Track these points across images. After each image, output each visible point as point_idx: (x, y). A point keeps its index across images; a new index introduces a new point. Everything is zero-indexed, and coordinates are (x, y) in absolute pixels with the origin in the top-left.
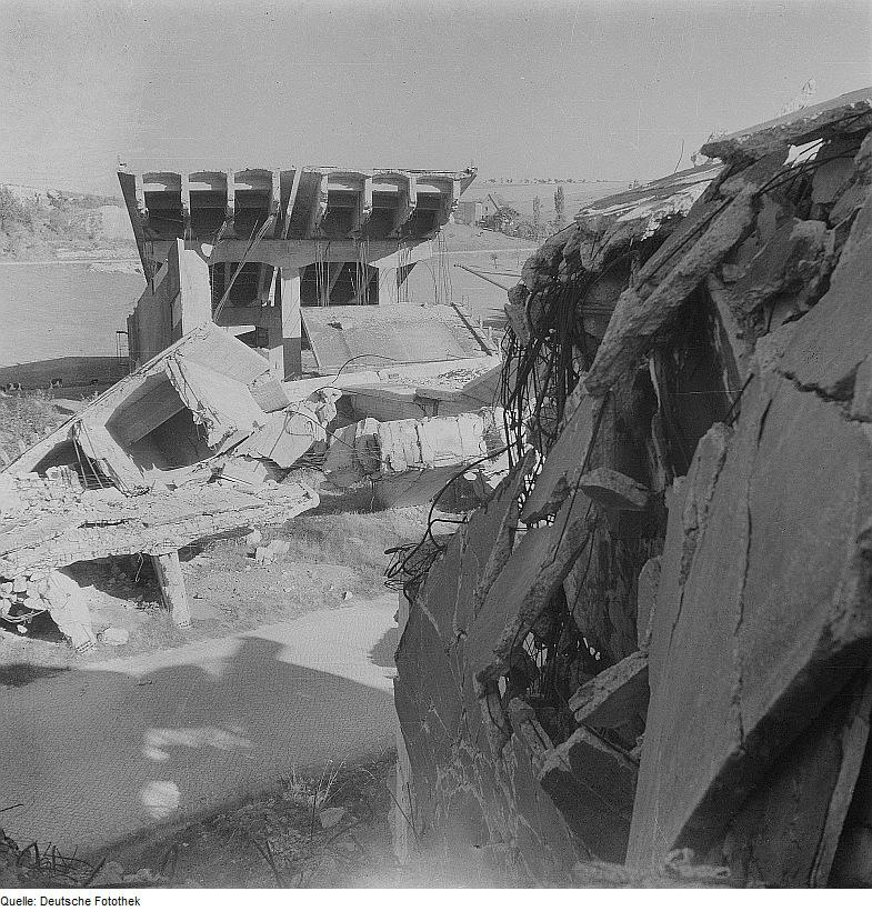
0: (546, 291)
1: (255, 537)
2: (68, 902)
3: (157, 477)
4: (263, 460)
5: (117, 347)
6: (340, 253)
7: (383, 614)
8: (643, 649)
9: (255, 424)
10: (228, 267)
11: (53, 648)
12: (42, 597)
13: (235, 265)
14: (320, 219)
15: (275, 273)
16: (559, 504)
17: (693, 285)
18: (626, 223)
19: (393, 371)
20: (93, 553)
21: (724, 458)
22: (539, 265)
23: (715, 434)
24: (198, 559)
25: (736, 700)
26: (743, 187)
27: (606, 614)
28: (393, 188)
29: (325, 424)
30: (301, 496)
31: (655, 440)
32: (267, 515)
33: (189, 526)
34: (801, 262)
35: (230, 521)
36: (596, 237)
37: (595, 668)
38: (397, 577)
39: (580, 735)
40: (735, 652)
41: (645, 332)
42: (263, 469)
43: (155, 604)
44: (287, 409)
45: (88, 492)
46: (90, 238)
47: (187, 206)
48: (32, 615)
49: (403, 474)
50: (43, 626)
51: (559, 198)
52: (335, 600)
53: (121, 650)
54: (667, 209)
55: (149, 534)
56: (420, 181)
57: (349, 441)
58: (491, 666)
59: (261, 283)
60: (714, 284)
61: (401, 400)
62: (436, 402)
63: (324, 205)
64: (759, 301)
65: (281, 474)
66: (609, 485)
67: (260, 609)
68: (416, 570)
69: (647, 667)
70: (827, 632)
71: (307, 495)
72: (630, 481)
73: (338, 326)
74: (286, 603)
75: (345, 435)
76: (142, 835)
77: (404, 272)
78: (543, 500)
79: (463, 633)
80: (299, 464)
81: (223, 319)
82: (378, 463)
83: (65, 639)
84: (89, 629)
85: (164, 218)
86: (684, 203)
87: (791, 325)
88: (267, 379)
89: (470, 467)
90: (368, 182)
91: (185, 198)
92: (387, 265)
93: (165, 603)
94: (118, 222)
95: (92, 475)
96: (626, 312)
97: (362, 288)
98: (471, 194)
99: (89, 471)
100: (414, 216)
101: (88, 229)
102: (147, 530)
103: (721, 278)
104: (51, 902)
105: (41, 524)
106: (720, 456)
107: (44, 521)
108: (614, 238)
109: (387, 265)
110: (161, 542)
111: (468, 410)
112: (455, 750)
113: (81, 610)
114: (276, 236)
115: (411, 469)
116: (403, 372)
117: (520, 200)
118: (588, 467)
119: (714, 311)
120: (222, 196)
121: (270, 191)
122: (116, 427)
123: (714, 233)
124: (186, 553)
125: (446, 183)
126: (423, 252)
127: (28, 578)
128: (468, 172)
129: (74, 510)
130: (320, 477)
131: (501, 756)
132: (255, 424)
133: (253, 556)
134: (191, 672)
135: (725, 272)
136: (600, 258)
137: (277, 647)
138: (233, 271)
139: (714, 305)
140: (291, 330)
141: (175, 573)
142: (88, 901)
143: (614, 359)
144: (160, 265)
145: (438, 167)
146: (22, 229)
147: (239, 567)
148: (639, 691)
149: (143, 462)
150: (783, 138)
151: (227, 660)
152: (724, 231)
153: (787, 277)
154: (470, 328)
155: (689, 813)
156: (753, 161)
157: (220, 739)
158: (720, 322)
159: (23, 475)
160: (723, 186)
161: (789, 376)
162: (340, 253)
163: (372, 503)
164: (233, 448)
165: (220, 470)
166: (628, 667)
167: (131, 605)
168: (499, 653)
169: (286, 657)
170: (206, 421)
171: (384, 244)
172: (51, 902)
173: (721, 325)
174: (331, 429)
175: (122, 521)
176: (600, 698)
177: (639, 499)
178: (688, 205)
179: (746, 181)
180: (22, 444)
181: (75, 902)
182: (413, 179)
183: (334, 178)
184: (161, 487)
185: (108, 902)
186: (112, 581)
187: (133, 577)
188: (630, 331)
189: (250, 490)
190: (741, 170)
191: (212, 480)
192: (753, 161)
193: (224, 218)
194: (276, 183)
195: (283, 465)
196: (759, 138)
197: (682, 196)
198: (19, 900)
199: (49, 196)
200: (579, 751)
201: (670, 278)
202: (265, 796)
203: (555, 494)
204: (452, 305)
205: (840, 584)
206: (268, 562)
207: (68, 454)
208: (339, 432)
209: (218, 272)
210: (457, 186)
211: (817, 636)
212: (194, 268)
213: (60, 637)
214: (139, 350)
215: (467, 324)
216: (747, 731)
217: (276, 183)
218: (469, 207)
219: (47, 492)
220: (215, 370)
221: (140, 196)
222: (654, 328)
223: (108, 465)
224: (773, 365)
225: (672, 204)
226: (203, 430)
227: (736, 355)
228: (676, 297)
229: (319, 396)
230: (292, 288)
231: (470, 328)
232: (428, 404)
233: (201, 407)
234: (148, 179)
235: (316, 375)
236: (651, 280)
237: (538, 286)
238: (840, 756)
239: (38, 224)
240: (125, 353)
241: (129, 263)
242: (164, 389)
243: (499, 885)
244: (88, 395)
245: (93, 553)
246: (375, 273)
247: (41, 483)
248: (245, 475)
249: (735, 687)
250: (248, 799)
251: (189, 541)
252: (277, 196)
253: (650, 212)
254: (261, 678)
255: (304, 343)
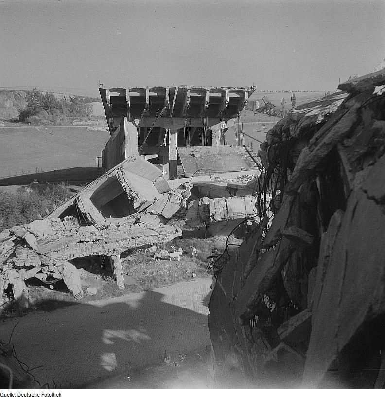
0: (276, 145)
1: (154, 248)
2: (30, 395)
3: (112, 221)
4: (158, 214)
6: (195, 123)
7: (205, 285)
9: (155, 199)
10: (146, 129)
11: (64, 295)
12: (60, 273)
13: (149, 129)
14: (186, 108)
15: (167, 132)
16: (277, 241)
18: (309, 117)
19: (217, 175)
20: (83, 254)
21: (340, 226)
22: (274, 134)
24: (129, 258)
26: (355, 104)
28: (219, 95)
29: (186, 199)
30: (173, 231)
34: (376, 139)
35: (142, 241)
36: (296, 122)
37: (294, 313)
39: (281, 345)
42: (158, 219)
44: (169, 192)
45: (82, 227)
46: (87, 116)
47: (129, 102)
48: (56, 281)
49: (219, 222)
50: (61, 286)
51: (293, 99)
52: (188, 277)
53: (93, 297)
54: (327, 111)
55: (107, 247)
56: (230, 92)
58: (246, 312)
59: (160, 137)
60: (340, 147)
63: (188, 102)
64: (358, 156)
65: (165, 221)
67: (155, 280)
68: (220, 265)
69: (310, 318)
70: (371, 308)
71: (177, 231)
72: (305, 233)
73: (194, 156)
74: (167, 278)
75: (194, 204)
77: (223, 132)
80: (174, 216)
81: (143, 152)
82: (209, 217)
83: (70, 292)
84: (80, 288)
85: (118, 108)
86: (333, 108)
87: (371, 167)
88: (161, 179)
90: (208, 92)
91: (128, 99)
92: (216, 128)
93: (114, 277)
94: (99, 109)
95: (84, 220)
96: (305, 156)
97: (205, 139)
98: (253, 97)
99: (82, 219)
101: (86, 112)
102: (107, 245)
103: (343, 144)
104: (22, 395)
106: (338, 224)
107: (62, 240)
108: (304, 123)
109: (216, 128)
110: (113, 250)
111: (248, 194)
113: (77, 280)
114: (167, 116)
115: (223, 220)
117: (276, 100)
118: (287, 225)
119: (339, 159)
120: (144, 98)
121: (165, 97)
123: (339, 125)
124: (123, 255)
125: (242, 93)
126: (231, 123)
127: (55, 265)
130: (183, 222)
134: (124, 306)
135: (345, 142)
136: (298, 131)
137: (161, 295)
139: (340, 156)
140: (173, 157)
141: (119, 264)
142: (39, 394)
143: (296, 179)
144: (116, 128)
145: (238, 86)
146: (59, 112)
147: (147, 262)
148: (307, 327)
149: (106, 214)
150: (373, 83)
151: (139, 301)
152: (343, 126)
154: (252, 157)
156: (360, 92)
158: (343, 164)
159: (54, 220)
161: (366, 192)
162: (195, 123)
163: (206, 234)
164: (145, 209)
166: (304, 315)
167: (99, 277)
169: (166, 300)
170: (133, 197)
171: (213, 120)
172: (22, 395)
174: (188, 202)
175: (96, 241)
176: (290, 329)
178: (336, 109)
180: (55, 206)
181: (33, 395)
182: (227, 91)
183: (193, 91)
184: (113, 226)
185: (47, 395)
186: (91, 266)
187: (100, 265)
190: (354, 97)
191: (135, 223)
192: (360, 92)
193: (144, 107)
194: (167, 93)
195: (167, 215)
196: (363, 82)
198: (8, 394)
201: (321, 144)
203: (275, 236)
207: (74, 211)
208: (192, 203)
209: (141, 132)
210: (247, 94)
212: (131, 130)
213: (68, 291)
214: (106, 167)
217: (167, 93)
218: (253, 103)
219: (64, 228)
220: (138, 176)
221: (108, 98)
222: (314, 166)
223: (91, 216)
224: (359, 186)
225: (329, 108)
226: (132, 202)
227: (349, 179)
228: (323, 153)
229: (183, 187)
230: (173, 138)
231: (252, 157)
232: (232, 191)
233: (131, 191)
234: (112, 90)
235: (183, 177)
236: (316, 144)
237: (273, 143)
239: (65, 110)
240: (101, 166)
241: (103, 127)
242: (115, 183)
245: (83, 254)
247: (61, 223)
248: (150, 222)
249: (337, 330)
251: (124, 250)
252: (168, 98)
255: (178, 162)
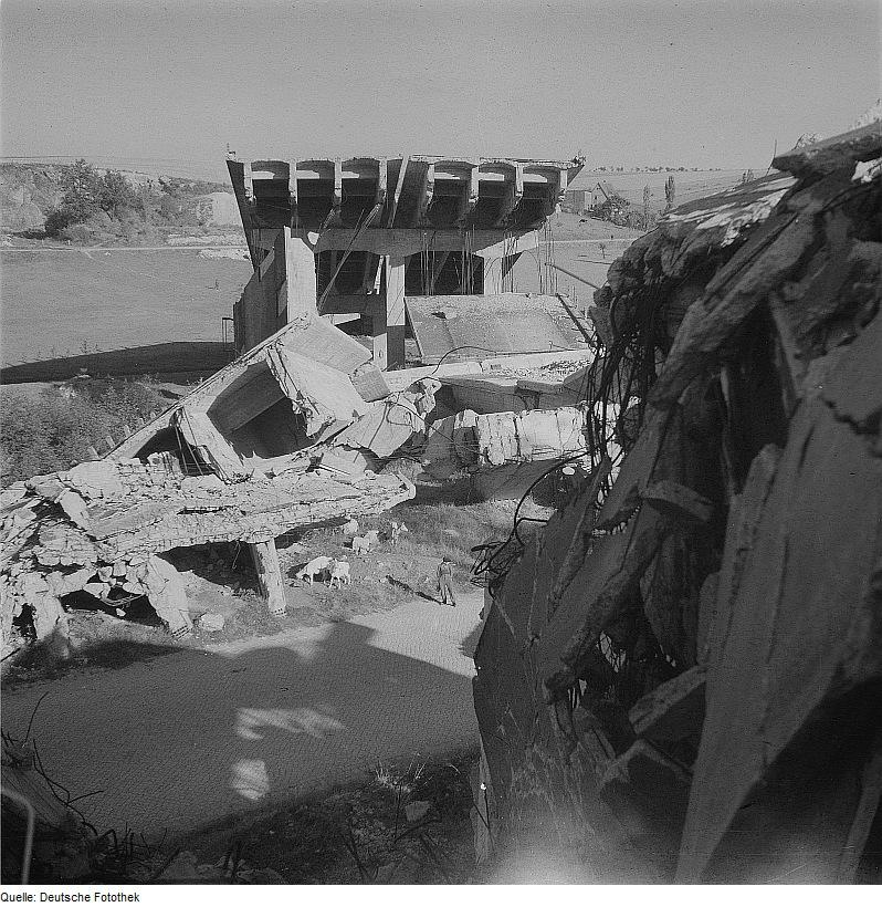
0: (631, 294)
1: (352, 526)
3: (257, 465)
4: (362, 449)
5: (219, 331)
6: (446, 242)
7: (470, 609)
8: (702, 663)
9: (355, 414)
10: (334, 255)
11: (150, 632)
12: (140, 581)
13: (340, 254)
14: (426, 208)
15: (381, 261)
17: (753, 304)
18: (704, 230)
21: (772, 482)
22: (624, 268)
23: (766, 456)
24: (296, 547)
25: (762, 730)
26: (811, 204)
27: (680, 621)
28: (500, 177)
29: (424, 415)
30: (397, 487)
31: (726, 452)
32: (362, 506)
33: (286, 515)
34: (856, 285)
35: (325, 511)
36: (675, 243)
37: (669, 674)
38: (483, 575)
39: (638, 747)
40: (765, 681)
41: (707, 348)
43: (252, 591)
45: (189, 479)
47: (294, 194)
48: (131, 599)
50: (141, 610)
53: (216, 636)
54: (746, 218)
55: (245, 523)
56: (526, 171)
57: (447, 433)
60: (775, 302)
61: (502, 391)
62: (537, 395)
63: (430, 194)
65: (378, 464)
66: (673, 499)
68: (503, 566)
70: (840, 671)
71: (404, 486)
72: (693, 495)
73: (442, 316)
74: (380, 593)
75: (443, 427)
76: (231, 821)
77: (509, 262)
78: (617, 506)
79: (537, 637)
80: (398, 454)
81: (326, 307)
84: (185, 615)
85: (271, 206)
87: (845, 349)
89: (568, 461)
90: (475, 171)
92: (492, 254)
93: (262, 591)
94: (226, 208)
96: (695, 321)
98: (577, 184)
99: (189, 459)
100: (520, 205)
101: (198, 215)
103: (781, 296)
104: (50, 898)
105: (142, 510)
106: (768, 477)
107: (145, 506)
108: (695, 245)
109: (492, 254)
110: (260, 530)
112: (528, 753)
113: (177, 597)
115: (509, 463)
116: (507, 363)
121: (377, 180)
122: (215, 414)
124: (282, 541)
125: (553, 173)
126: (529, 241)
127: (128, 563)
128: (575, 161)
129: (173, 497)
130: (418, 468)
131: (568, 762)
132: (355, 414)
133: (350, 545)
134: (285, 655)
135: (786, 290)
136: (680, 264)
137: (370, 632)
138: (339, 259)
140: (395, 318)
141: (273, 563)
142: (88, 897)
143: (677, 373)
144: (267, 252)
145: (545, 157)
146: (134, 216)
148: (695, 705)
149: (243, 450)
150: (851, 153)
151: (320, 643)
152: (783, 253)
153: (843, 300)
154: (574, 318)
155: (718, 839)
157: (310, 720)
159: (125, 461)
160: (792, 202)
161: (831, 405)
162: (446, 242)
163: (470, 495)
165: (319, 460)
166: (688, 681)
167: (227, 591)
168: (566, 661)
169: (379, 642)
170: (305, 410)
173: (780, 344)
174: (429, 421)
175: (220, 509)
176: (659, 711)
177: (702, 512)
178: (766, 212)
179: (812, 197)
181: (75, 898)
182: (520, 168)
183: (440, 167)
184: (259, 475)
185: (108, 897)
186: (210, 567)
187: (229, 564)
188: (691, 347)
189: (348, 480)
191: (310, 469)
193: (330, 206)
194: (383, 172)
195: (383, 451)
196: (829, 154)
197: (761, 204)
198: (19, 897)
199: (162, 183)
200: (638, 762)
202: (353, 786)
204: (557, 295)
205: (853, 622)
206: (364, 552)
207: (170, 441)
208: (438, 423)
209: (324, 261)
210: (564, 176)
211: (831, 674)
212: (300, 257)
214: (243, 341)
215: (571, 315)
216: (769, 761)
217: (383, 172)
218: (578, 196)
220: (317, 361)
221: (248, 184)
225: (751, 212)
226: (302, 420)
228: (736, 315)
230: (396, 276)
231: (574, 318)
232: (529, 397)
233: (300, 396)
234: (257, 167)
235: (419, 364)
236: (719, 293)
237: (623, 289)
238: (860, 793)
239: (150, 209)
242: (264, 378)
243: (574, 883)
244: (194, 380)
246: (480, 262)
247: (143, 469)
250: (338, 788)
251: (285, 530)
252: (383, 185)
253: (729, 220)
254: (353, 665)
255: (408, 331)
